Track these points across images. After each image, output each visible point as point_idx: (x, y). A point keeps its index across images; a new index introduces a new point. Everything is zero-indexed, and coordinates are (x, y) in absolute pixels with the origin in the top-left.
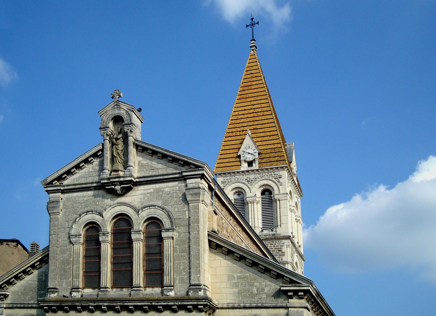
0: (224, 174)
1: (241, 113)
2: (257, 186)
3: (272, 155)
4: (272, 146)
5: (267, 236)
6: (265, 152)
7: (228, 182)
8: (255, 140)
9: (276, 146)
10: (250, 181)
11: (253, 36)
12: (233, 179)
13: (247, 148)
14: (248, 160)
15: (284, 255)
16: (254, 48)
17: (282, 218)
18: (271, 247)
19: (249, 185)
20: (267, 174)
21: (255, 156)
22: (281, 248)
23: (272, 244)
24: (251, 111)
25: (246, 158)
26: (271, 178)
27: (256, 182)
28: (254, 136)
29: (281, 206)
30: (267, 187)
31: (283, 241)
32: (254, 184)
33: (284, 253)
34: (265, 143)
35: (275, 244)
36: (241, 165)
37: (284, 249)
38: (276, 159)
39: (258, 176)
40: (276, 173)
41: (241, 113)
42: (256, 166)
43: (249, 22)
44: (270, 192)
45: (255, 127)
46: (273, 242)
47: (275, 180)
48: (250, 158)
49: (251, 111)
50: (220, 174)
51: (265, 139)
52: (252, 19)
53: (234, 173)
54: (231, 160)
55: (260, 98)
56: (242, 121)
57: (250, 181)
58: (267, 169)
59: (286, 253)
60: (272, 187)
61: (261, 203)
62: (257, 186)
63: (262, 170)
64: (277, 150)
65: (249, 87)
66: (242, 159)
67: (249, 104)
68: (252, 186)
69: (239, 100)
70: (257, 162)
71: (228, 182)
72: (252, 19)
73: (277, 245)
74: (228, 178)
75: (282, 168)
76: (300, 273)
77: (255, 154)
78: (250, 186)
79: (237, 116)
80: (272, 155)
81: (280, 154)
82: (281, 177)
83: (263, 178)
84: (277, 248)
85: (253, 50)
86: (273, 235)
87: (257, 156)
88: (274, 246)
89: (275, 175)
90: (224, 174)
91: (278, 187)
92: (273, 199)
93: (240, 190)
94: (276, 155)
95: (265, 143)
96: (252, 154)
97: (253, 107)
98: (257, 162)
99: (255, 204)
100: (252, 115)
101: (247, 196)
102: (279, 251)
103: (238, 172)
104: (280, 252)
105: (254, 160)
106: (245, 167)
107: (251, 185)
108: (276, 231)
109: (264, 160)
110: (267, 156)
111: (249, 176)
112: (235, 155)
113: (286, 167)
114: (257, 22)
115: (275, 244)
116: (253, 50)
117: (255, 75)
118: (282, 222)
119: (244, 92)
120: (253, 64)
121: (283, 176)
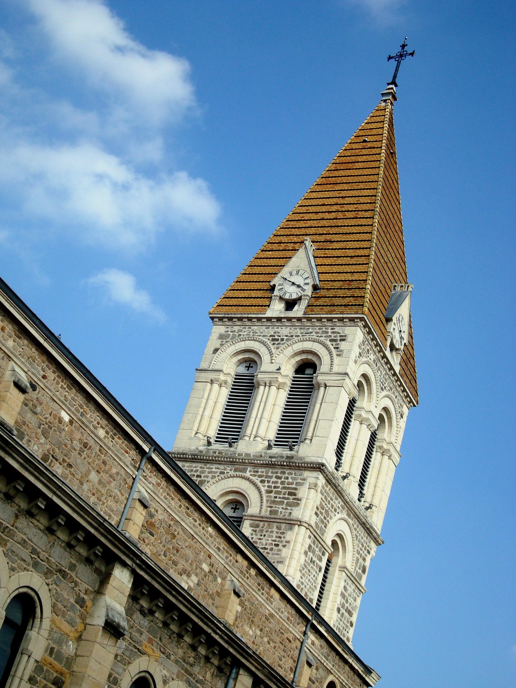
0: (230, 319)
1: (311, 209)
2: (289, 351)
3: (340, 293)
4: (349, 277)
5: (274, 457)
6: (329, 285)
7: (233, 338)
8: (320, 261)
9: (356, 277)
10: (277, 340)
11: (395, 77)
12: (245, 332)
13: (294, 273)
14: (287, 297)
15: (298, 505)
16: (390, 97)
17: (321, 423)
18: (276, 482)
19: (272, 348)
20: (317, 330)
21: (304, 290)
22: (296, 489)
23: (280, 478)
24: (334, 208)
25: (285, 293)
26: (322, 339)
27: (289, 343)
28: (321, 253)
29: (327, 399)
30: (310, 357)
31: (306, 474)
32: (284, 346)
33: (300, 500)
34: (335, 269)
35: (287, 478)
36: (269, 306)
37: (303, 492)
38: (346, 301)
39: (298, 331)
40: (337, 329)
41: (311, 209)
42: (298, 311)
43: (396, 50)
44: (313, 366)
45: (328, 237)
46: (284, 473)
47: (329, 343)
48: (292, 293)
49: (334, 208)
50: (221, 319)
51: (340, 261)
52: (403, 46)
53: (250, 319)
54: (253, 294)
55: (362, 186)
56: (309, 224)
57: (277, 340)
58: (320, 319)
59: (303, 501)
60: (319, 358)
61: (288, 389)
62: (289, 351)
63: (309, 319)
64: (354, 285)
65: (350, 165)
66: (276, 292)
67: (336, 194)
68: (279, 350)
69: (319, 187)
70: (304, 303)
71: (233, 338)
72: (403, 46)
73: (290, 480)
74: (236, 328)
75: (352, 320)
76: (219, 506)
77: (305, 287)
78: (274, 351)
79: (301, 215)
80: (340, 293)
81: (357, 293)
82: (344, 340)
83: (307, 337)
84: (288, 488)
85: (385, 101)
86: (288, 457)
87: (309, 291)
88: (283, 483)
89: (333, 333)
90: (230, 319)
91: (332, 359)
92: (314, 382)
93: (252, 356)
94: (349, 293)
95: (335, 269)
96: (299, 286)
97: (341, 201)
98: (304, 303)
99: (274, 389)
100: (333, 215)
101: (262, 369)
102: (290, 494)
103: (259, 319)
104: (291, 497)
105: (300, 299)
106: (277, 309)
107: (278, 348)
108: (297, 452)
109: (320, 302)
110: (331, 293)
111: (279, 330)
112: (266, 286)
113: (362, 319)
114: (410, 52)
115: (287, 478)
116: (385, 101)
117: (369, 145)
118: (317, 433)
119: (336, 173)
120: (374, 126)
121: (349, 339)
